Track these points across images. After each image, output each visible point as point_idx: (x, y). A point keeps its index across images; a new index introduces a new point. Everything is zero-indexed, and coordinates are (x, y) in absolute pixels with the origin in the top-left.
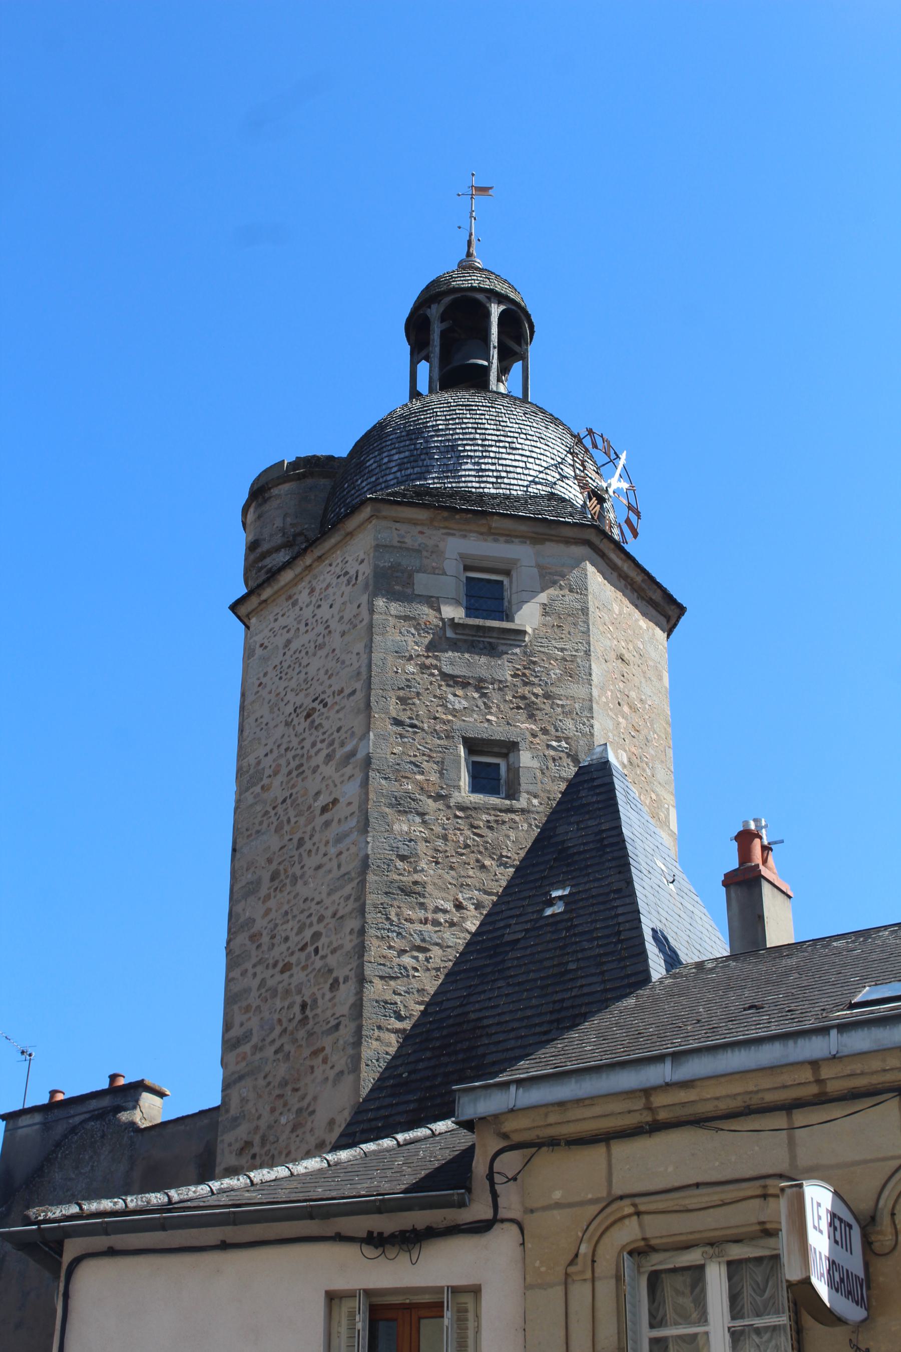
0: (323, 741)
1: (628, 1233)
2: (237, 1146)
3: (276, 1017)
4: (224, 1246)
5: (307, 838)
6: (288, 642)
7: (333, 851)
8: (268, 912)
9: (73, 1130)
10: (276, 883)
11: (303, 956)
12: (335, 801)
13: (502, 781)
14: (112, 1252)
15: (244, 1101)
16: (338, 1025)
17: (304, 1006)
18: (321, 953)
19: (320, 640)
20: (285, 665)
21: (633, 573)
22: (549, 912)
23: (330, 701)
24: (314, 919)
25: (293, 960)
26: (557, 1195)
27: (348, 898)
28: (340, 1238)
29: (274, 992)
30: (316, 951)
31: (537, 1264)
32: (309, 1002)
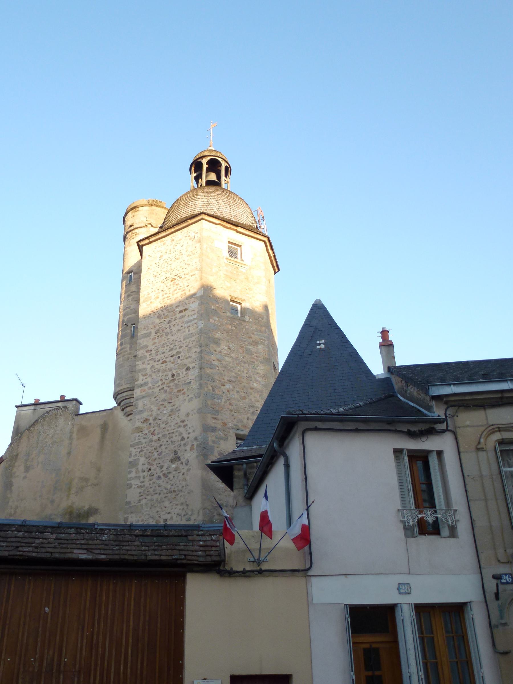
0: (179, 289)
1: (497, 436)
2: (143, 420)
3: (160, 378)
4: (357, 430)
5: (173, 320)
6: (161, 256)
7: (186, 325)
8: (155, 343)
9: (47, 413)
10: (158, 334)
11: (172, 359)
12: (186, 310)
13: (239, 312)
14: (316, 429)
15: (145, 405)
16: (190, 382)
17: (173, 375)
18: (181, 358)
19: (177, 257)
20: (160, 264)
21: (272, 255)
22: (318, 347)
23: (183, 277)
24: (178, 347)
25: (167, 360)
26: (468, 423)
27: (194, 341)
28: (396, 431)
29: (159, 371)
30: (179, 357)
31: (464, 445)
32: (175, 374)
